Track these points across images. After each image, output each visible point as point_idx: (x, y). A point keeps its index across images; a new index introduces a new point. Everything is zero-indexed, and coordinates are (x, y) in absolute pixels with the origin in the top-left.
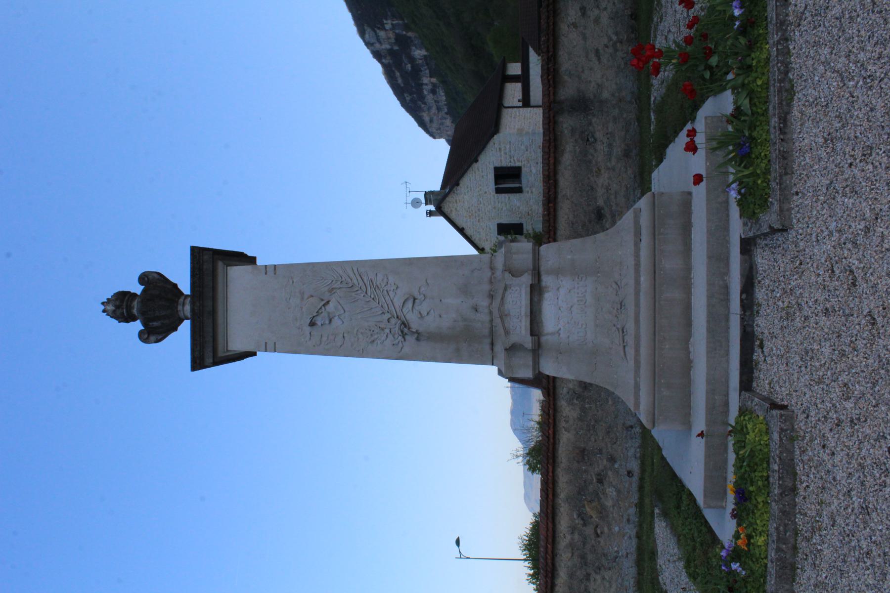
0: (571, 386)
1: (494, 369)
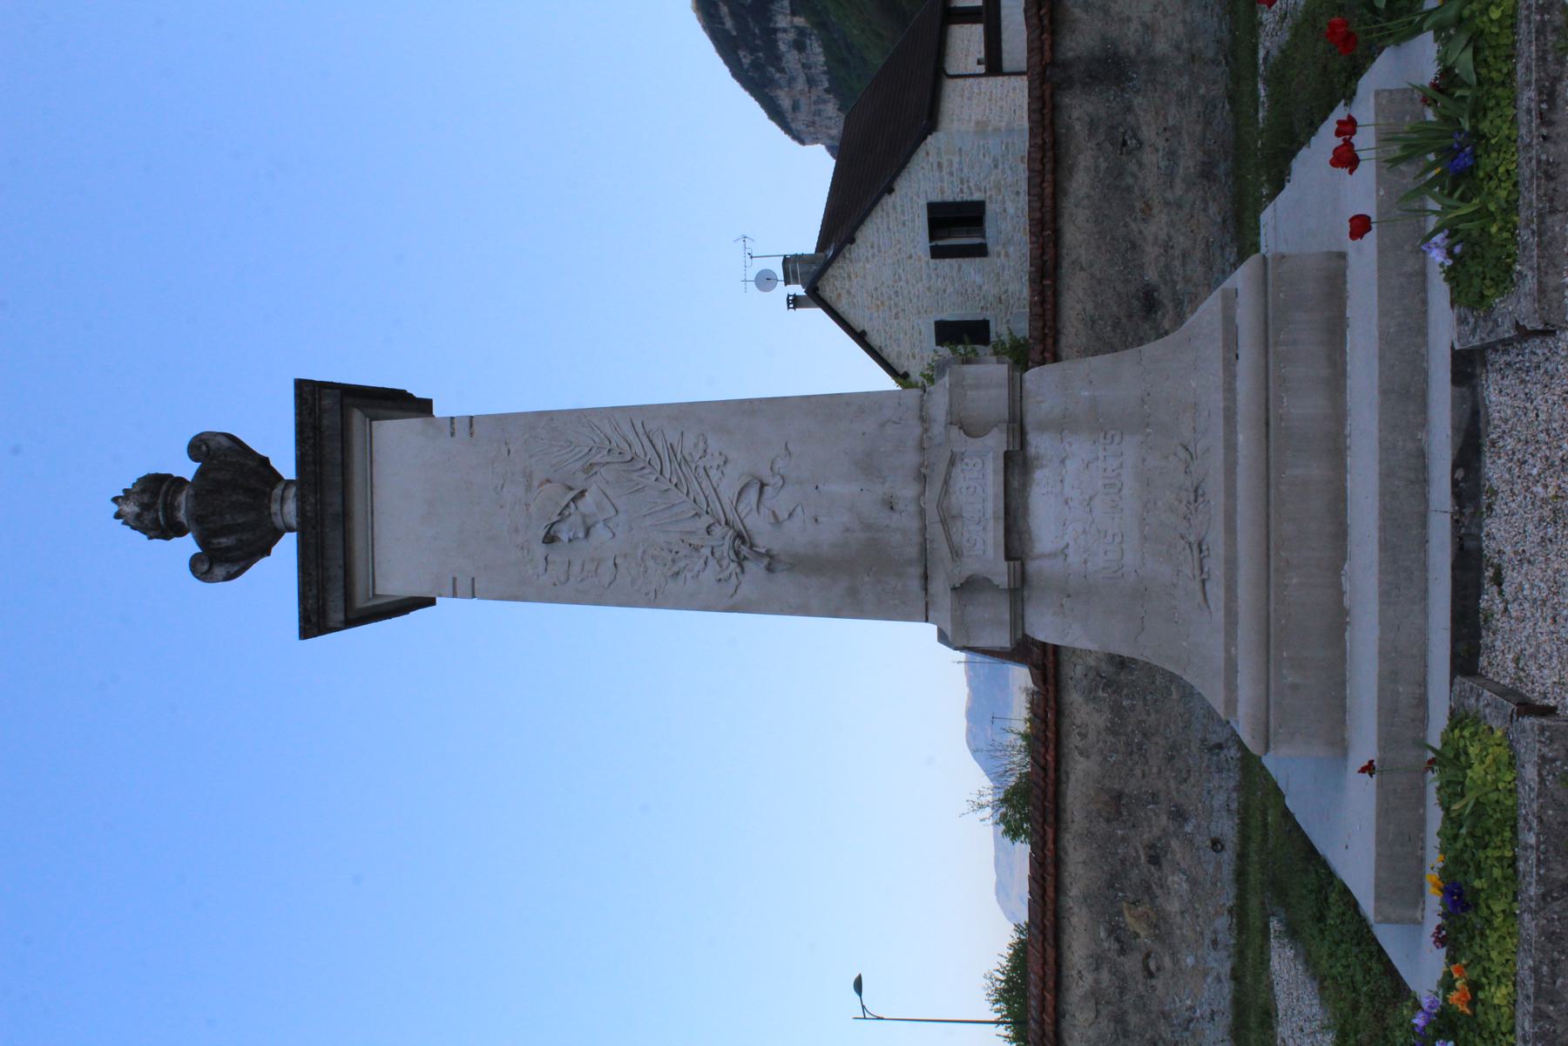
0: (1091, 662)
1: (930, 630)
